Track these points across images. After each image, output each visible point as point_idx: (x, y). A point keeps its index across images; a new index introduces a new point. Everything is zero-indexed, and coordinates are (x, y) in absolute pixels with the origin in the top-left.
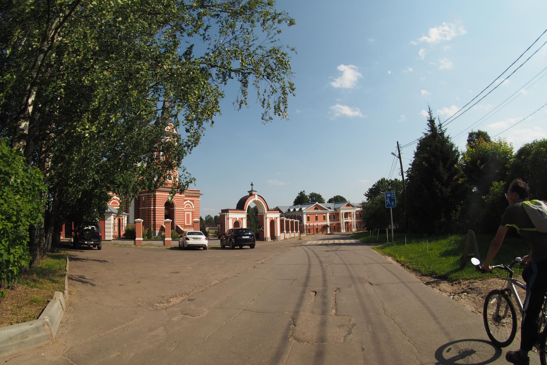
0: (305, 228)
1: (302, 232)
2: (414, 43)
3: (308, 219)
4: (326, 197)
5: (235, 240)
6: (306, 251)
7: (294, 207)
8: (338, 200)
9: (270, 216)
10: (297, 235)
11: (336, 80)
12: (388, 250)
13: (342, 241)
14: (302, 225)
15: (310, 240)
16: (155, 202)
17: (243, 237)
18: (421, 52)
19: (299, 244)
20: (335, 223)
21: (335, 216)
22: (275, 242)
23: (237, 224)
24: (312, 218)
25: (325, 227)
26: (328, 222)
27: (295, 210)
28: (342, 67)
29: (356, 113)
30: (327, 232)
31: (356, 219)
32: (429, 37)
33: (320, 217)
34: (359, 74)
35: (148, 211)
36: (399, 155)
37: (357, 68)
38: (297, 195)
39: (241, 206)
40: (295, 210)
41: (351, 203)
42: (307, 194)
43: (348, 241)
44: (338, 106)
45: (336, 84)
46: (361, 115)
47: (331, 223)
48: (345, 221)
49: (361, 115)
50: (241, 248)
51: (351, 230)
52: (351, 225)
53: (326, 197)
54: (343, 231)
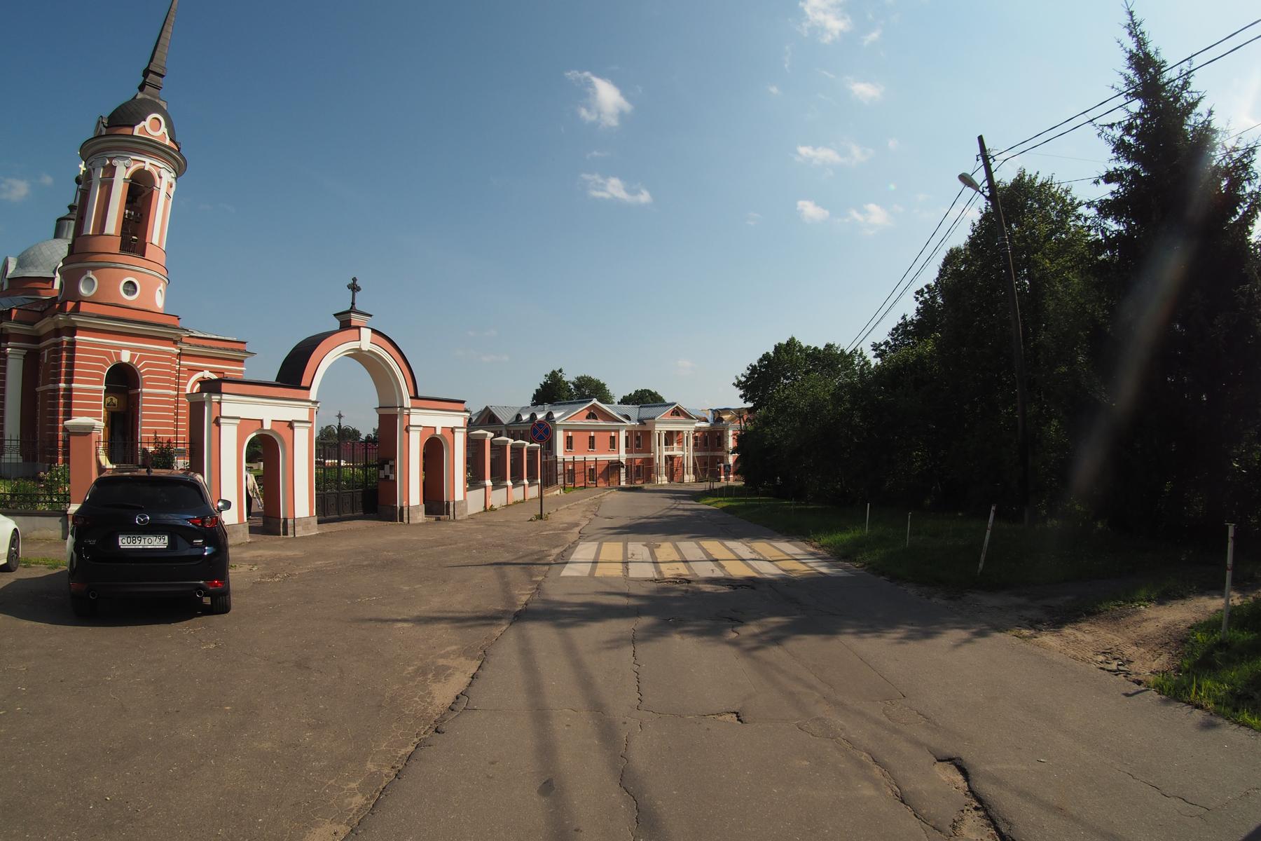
0: (560, 468)
1: (548, 482)
3: (569, 443)
4: (618, 390)
7: (533, 409)
8: (644, 398)
10: (533, 492)
14: (551, 458)
16: (71, 366)
17: (124, 542)
20: (639, 457)
21: (640, 439)
22: (445, 529)
24: (581, 440)
25: (614, 467)
26: (622, 455)
27: (533, 416)
31: (695, 450)
38: (543, 380)
40: (533, 416)
41: (685, 405)
42: (569, 377)
47: (631, 456)
48: (666, 453)
53: (618, 390)
54: (663, 480)
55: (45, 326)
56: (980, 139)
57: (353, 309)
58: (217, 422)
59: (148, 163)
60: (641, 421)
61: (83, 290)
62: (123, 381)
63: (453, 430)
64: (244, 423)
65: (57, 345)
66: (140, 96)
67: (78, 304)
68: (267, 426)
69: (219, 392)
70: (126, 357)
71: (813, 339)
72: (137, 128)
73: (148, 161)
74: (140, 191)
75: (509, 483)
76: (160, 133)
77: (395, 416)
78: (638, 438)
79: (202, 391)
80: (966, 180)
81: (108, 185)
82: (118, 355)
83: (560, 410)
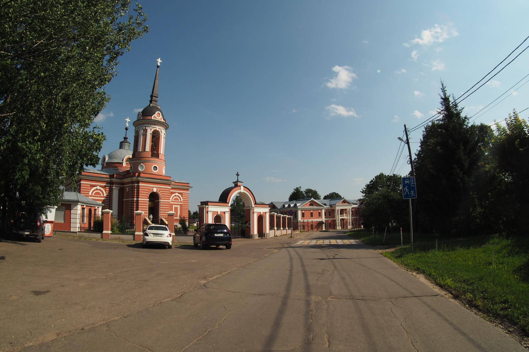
2: (407, 45)
4: (322, 194)
5: (209, 238)
6: (291, 259)
7: (290, 203)
8: (334, 196)
9: (258, 210)
10: (289, 232)
11: (331, 80)
12: (410, 258)
13: (340, 242)
15: (303, 239)
17: (216, 235)
18: (414, 54)
19: (286, 245)
21: (330, 213)
23: (218, 218)
24: (307, 214)
26: (323, 219)
27: (289, 205)
28: (337, 68)
29: (351, 113)
30: (322, 229)
32: (421, 39)
33: (315, 213)
34: (354, 75)
35: (131, 203)
36: (407, 140)
37: (352, 69)
38: (293, 191)
39: (223, 198)
40: (289, 205)
41: (347, 199)
42: (303, 190)
43: (347, 242)
44: (333, 106)
45: (331, 85)
46: (355, 115)
47: (327, 219)
48: (340, 218)
49: (355, 115)
50: (217, 249)
51: (347, 228)
52: (347, 222)
53: (322, 194)
54: (339, 228)
55: (126, 180)
56: (405, 125)
57: (238, 181)
58: (207, 212)
59: (158, 128)
60: (331, 206)
61: (140, 169)
62: (154, 197)
63: (266, 213)
64: (214, 212)
65: (132, 186)
66: (151, 105)
67: (139, 174)
68: (219, 213)
69: (208, 205)
70: (155, 190)
71: (388, 173)
72: (153, 116)
73: (157, 127)
74: (156, 136)
75: (282, 228)
76: (160, 118)
77: (250, 210)
78: (330, 212)
79: (201, 205)
80: (400, 139)
81: (145, 136)
82: (153, 190)
83: (299, 203)
